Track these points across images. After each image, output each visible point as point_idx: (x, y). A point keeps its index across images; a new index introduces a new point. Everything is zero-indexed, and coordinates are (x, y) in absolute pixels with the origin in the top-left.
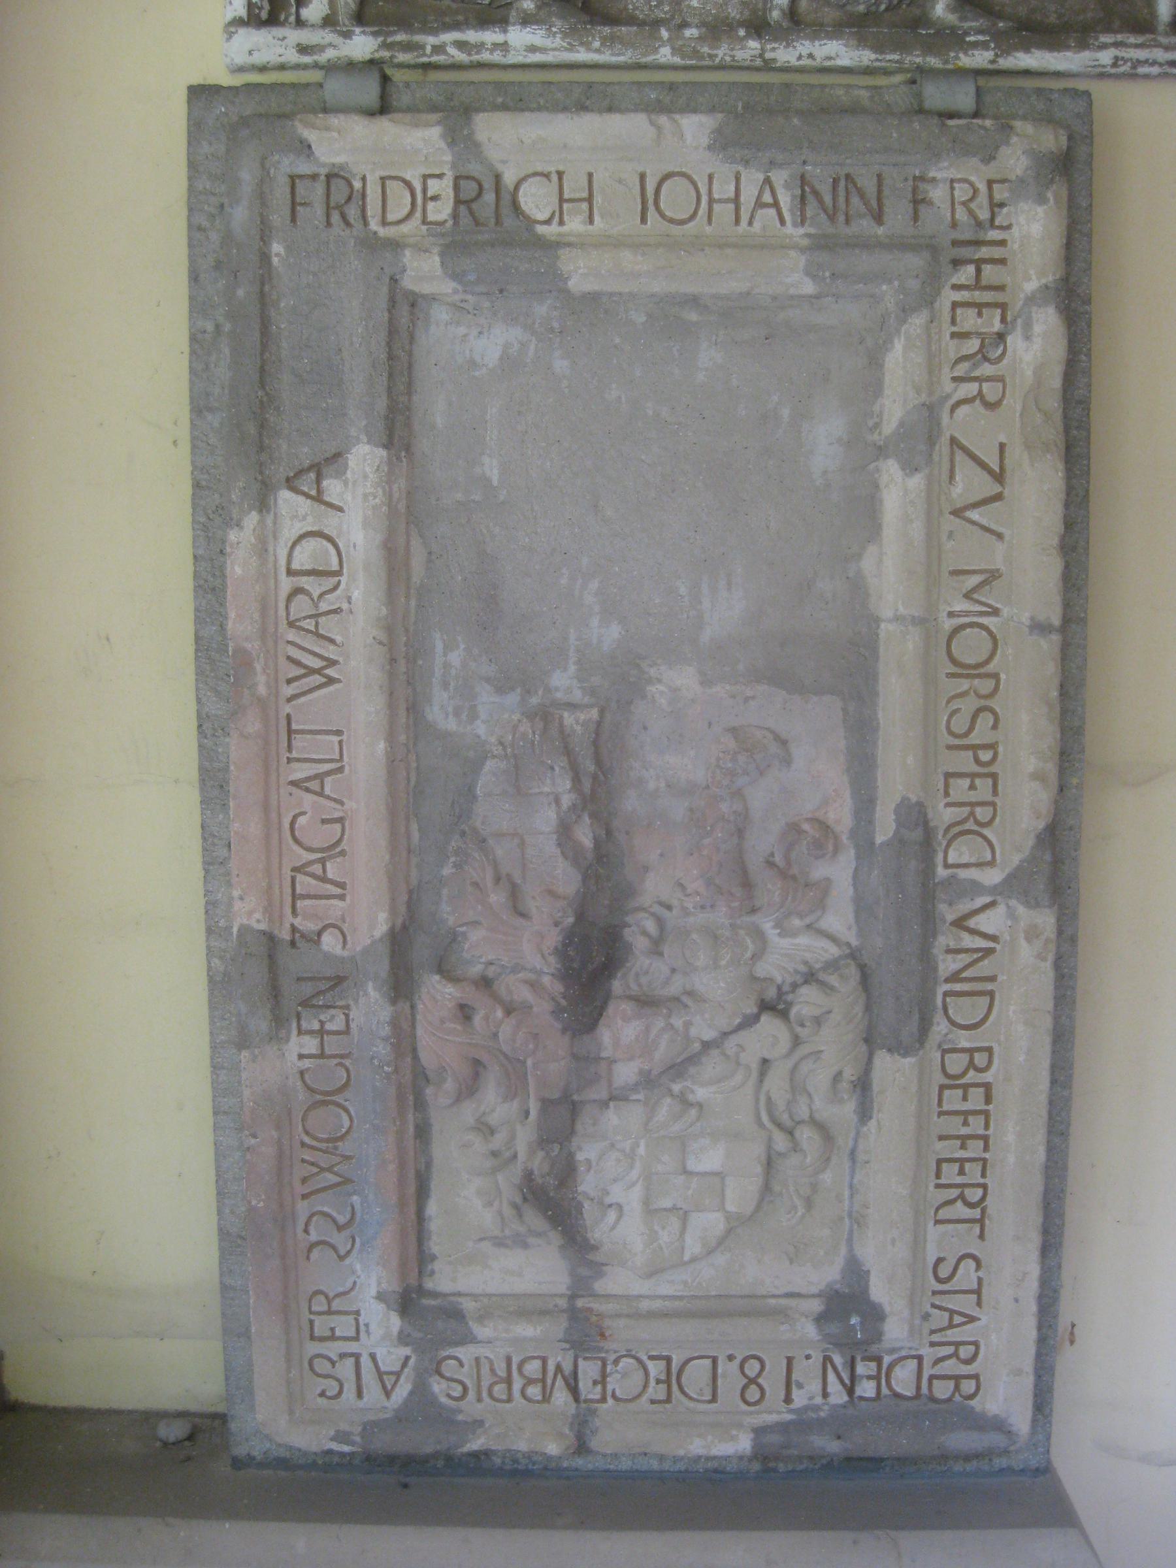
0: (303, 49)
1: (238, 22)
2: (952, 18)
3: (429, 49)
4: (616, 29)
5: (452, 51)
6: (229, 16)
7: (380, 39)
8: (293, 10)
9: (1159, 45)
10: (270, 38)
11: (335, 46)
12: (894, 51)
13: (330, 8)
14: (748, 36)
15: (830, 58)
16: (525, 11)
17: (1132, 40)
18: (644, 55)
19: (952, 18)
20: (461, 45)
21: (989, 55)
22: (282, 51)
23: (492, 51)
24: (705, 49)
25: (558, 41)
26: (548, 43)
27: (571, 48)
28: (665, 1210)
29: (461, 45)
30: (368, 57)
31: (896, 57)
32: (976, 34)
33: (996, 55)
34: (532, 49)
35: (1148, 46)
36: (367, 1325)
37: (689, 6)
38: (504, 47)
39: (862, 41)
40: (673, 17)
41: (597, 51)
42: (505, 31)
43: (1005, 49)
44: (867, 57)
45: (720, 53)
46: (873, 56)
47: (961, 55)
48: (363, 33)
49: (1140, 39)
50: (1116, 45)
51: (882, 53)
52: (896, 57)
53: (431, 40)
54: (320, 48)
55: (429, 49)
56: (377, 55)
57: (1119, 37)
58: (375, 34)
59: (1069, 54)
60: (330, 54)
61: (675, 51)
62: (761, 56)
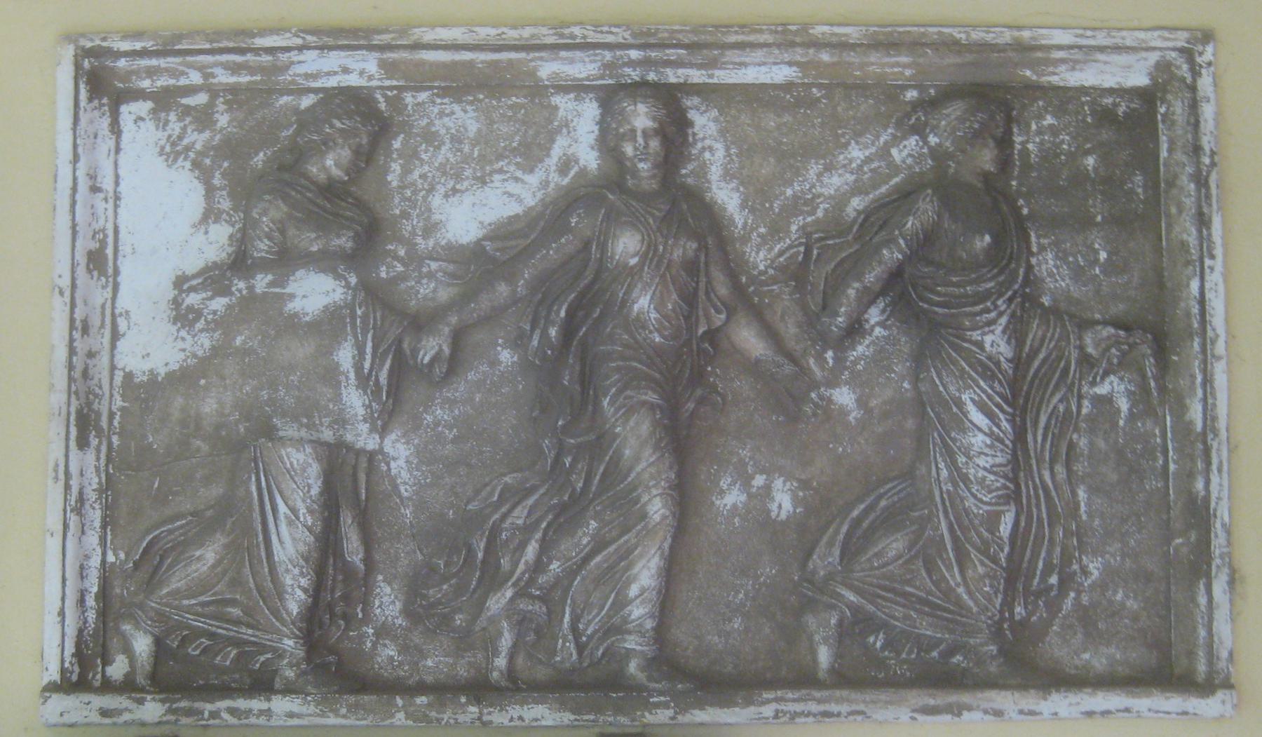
0: (104, 713)
1: (52, 688)
2: (641, 677)
3: (206, 714)
4: (359, 697)
5: (225, 716)
6: (45, 681)
7: (167, 705)
8: (100, 669)
9: (814, 699)
10: (77, 702)
11: (130, 711)
12: (588, 713)
13: (131, 666)
14: (469, 703)
15: (537, 720)
16: (286, 678)
17: (790, 695)
18: (383, 720)
19: (641, 677)
20: (233, 711)
21: (670, 713)
22: (85, 713)
23: (258, 716)
24: (433, 714)
25: (312, 708)
26: (304, 710)
27: (323, 715)
28: (1229, 381)
29: (233, 711)
30: (157, 720)
31: (592, 717)
32: (659, 695)
33: (676, 713)
34: (291, 715)
35: (805, 700)
36: (56, 479)
37: (424, 666)
38: (268, 713)
39: (563, 706)
40: (412, 675)
41: (344, 716)
42: (269, 700)
43: (682, 709)
44: (567, 717)
45: (446, 717)
46: (572, 717)
47: (647, 714)
48: (154, 699)
49: (797, 695)
50: (777, 700)
51: (579, 714)
52: (592, 717)
53: (209, 707)
54: (119, 712)
55: (206, 714)
56: (165, 719)
57: (779, 693)
58: (163, 701)
59: (737, 709)
60: (126, 717)
61: (408, 716)
62: (479, 719)
